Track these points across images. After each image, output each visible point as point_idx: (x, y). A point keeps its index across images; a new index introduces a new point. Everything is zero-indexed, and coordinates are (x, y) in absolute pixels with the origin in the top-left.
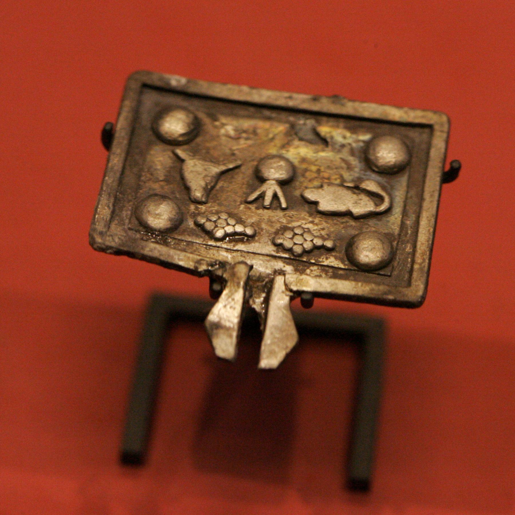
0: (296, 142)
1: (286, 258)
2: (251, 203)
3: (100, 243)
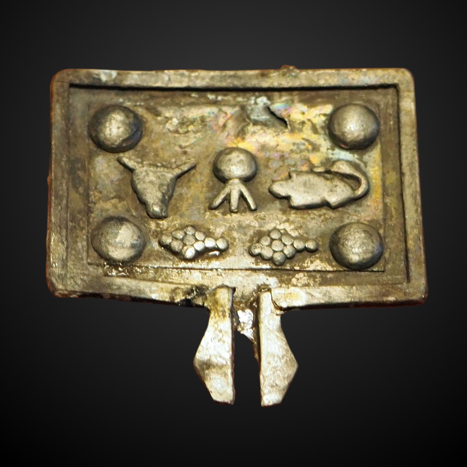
0: (251, 128)
1: (267, 269)
2: (216, 208)
3: (61, 290)
